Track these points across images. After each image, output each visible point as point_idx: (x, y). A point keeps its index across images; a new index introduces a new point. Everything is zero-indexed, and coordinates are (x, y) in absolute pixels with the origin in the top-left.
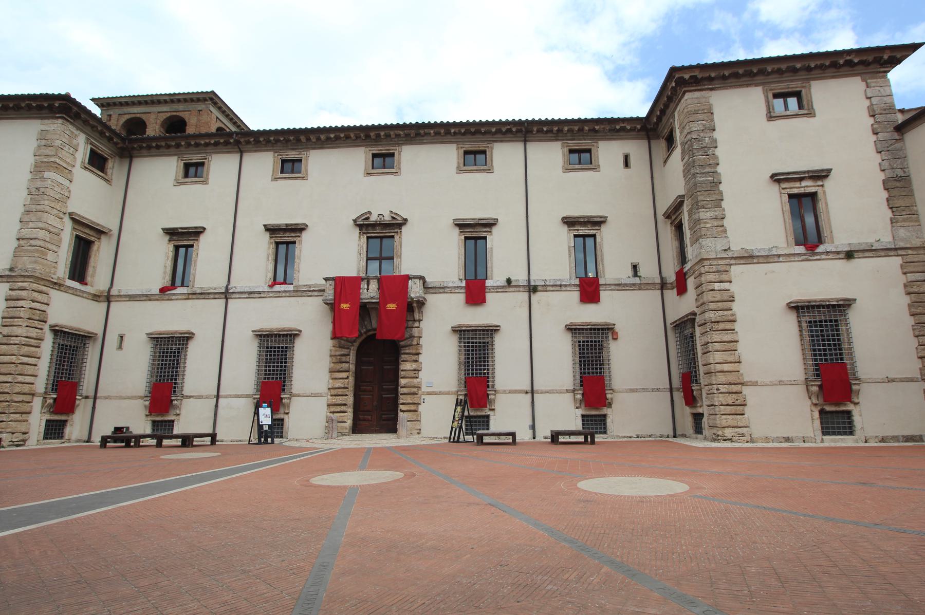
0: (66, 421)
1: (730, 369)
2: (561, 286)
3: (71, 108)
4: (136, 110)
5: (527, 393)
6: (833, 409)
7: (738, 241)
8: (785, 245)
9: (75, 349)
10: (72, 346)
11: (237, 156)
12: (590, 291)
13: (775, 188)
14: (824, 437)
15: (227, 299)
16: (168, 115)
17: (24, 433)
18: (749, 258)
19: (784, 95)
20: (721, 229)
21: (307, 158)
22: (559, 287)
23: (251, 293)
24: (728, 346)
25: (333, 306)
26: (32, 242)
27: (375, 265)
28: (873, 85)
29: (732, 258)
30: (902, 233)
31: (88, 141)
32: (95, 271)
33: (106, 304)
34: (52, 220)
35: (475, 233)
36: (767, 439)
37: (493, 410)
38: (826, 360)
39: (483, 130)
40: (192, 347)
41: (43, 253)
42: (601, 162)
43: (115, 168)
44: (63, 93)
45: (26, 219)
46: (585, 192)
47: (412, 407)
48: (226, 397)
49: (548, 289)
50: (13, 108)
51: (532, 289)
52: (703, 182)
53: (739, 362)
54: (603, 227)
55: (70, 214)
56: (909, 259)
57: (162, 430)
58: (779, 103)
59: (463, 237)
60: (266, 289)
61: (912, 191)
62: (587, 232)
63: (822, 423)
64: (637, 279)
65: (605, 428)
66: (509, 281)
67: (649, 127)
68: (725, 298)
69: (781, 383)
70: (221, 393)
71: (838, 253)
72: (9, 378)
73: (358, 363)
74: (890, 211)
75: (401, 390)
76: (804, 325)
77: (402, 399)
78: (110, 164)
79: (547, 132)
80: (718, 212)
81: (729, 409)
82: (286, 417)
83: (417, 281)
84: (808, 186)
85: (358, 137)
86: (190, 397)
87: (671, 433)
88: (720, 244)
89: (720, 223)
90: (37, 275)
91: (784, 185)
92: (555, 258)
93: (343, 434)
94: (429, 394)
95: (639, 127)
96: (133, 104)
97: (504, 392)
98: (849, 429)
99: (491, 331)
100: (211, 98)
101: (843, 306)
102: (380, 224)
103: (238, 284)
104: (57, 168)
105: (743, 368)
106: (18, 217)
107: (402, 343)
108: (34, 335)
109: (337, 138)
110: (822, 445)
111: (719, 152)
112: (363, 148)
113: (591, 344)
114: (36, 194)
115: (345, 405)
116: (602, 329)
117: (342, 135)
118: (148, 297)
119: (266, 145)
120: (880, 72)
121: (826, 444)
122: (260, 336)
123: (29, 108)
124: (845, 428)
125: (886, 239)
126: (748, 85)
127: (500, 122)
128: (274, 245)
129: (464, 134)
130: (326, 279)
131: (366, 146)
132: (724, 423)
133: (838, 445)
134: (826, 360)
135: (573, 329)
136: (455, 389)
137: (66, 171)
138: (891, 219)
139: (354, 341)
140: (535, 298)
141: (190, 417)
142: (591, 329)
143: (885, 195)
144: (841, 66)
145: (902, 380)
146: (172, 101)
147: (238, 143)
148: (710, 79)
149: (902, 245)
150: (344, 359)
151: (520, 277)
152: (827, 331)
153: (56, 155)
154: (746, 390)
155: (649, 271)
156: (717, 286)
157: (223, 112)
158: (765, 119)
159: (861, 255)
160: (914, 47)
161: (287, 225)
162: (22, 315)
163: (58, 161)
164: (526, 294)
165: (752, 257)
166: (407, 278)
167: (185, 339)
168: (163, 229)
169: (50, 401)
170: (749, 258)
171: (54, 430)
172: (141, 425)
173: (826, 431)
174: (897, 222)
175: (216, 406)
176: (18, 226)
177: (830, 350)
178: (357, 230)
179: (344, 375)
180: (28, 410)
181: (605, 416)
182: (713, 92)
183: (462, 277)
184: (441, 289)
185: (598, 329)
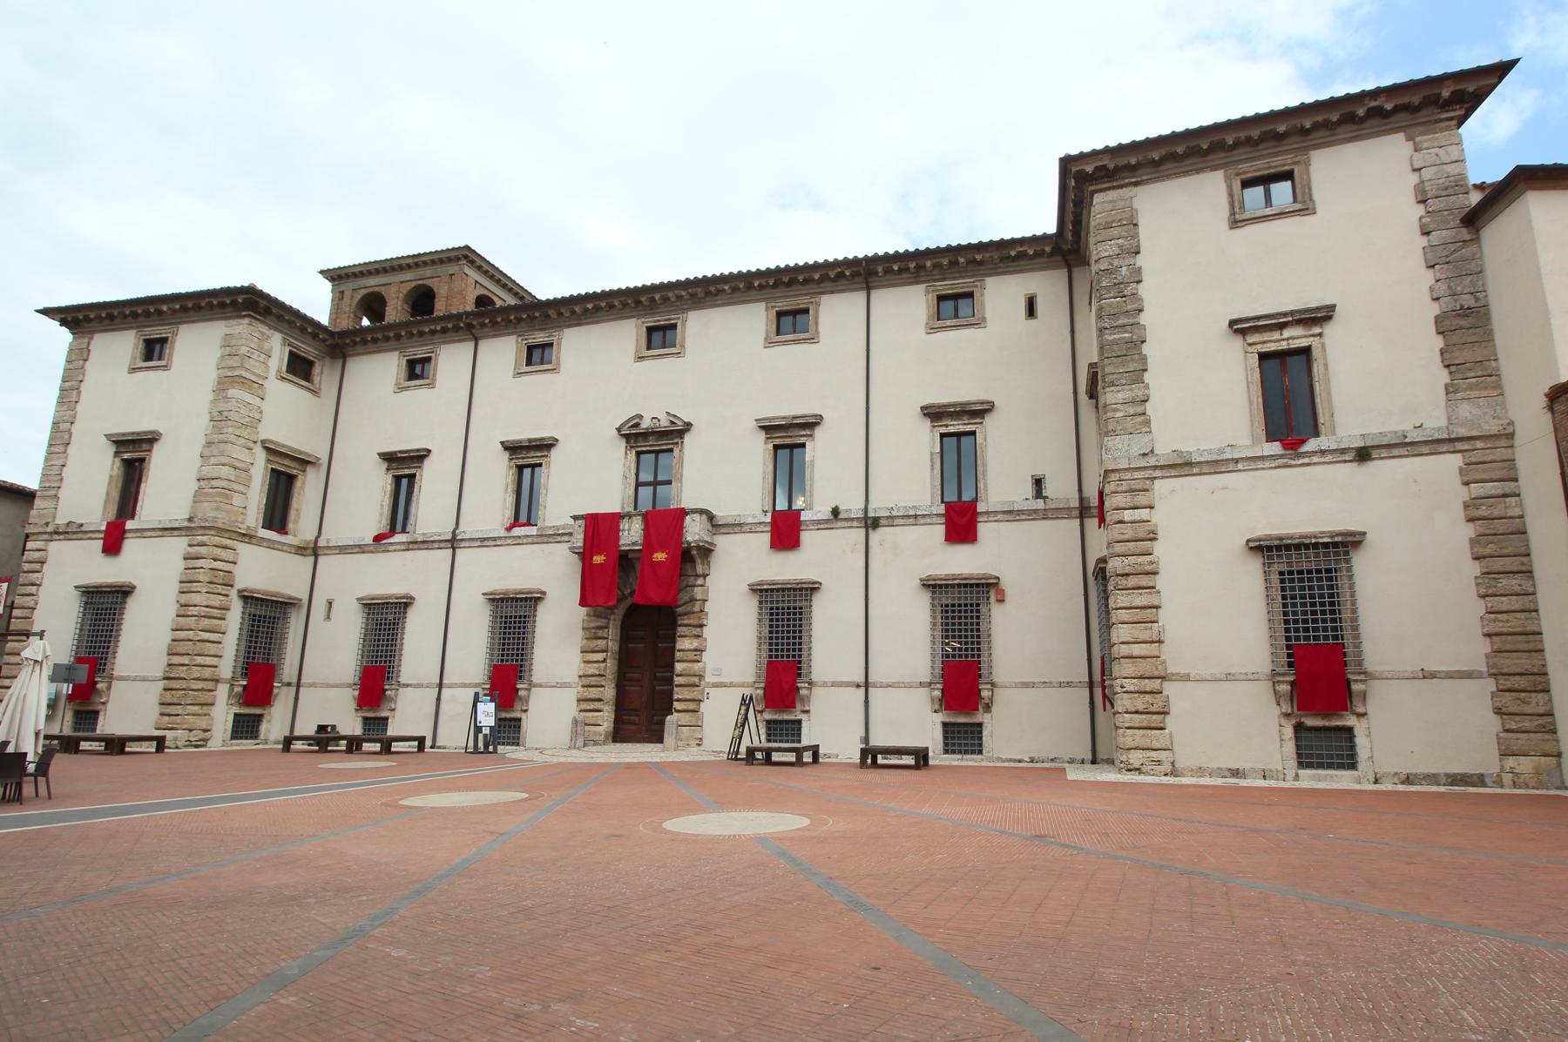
0: (261, 716)
1: (1143, 653)
2: (916, 516)
4: (373, 282)
7: (1168, 438)
8: (1248, 442)
10: (268, 616)
12: (961, 523)
13: (1237, 343)
15: (454, 549)
16: (413, 284)
17: (206, 731)
18: (1184, 466)
20: (1140, 419)
21: (560, 340)
22: (914, 518)
24: (1141, 615)
25: (585, 556)
26: (214, 483)
27: (646, 492)
28: (1425, 145)
29: (1155, 467)
30: (1465, 410)
32: (298, 516)
33: (312, 559)
34: (237, 452)
35: (788, 439)
36: (1200, 771)
37: (807, 712)
39: (801, 278)
40: (412, 614)
41: (226, 496)
42: (988, 315)
43: (325, 375)
46: (955, 364)
47: (691, 706)
48: (452, 686)
49: (897, 522)
51: (871, 523)
52: (1115, 342)
53: (1160, 642)
54: (988, 419)
55: (263, 442)
56: (1476, 457)
57: (374, 727)
58: (1255, 194)
59: (770, 446)
60: (503, 533)
61: (1490, 333)
64: (1040, 501)
65: (980, 745)
66: (835, 512)
67: (1065, 247)
68: (1141, 536)
69: (1229, 677)
71: (1343, 451)
72: (185, 660)
73: (625, 639)
74: (1446, 371)
75: (678, 680)
76: (1275, 577)
77: (678, 693)
78: (317, 369)
79: (900, 271)
80: (1138, 391)
82: (523, 716)
83: (697, 517)
84: (1296, 337)
85: (625, 305)
86: (407, 686)
87: (1089, 757)
88: (1137, 445)
89: (1139, 409)
91: (1251, 339)
92: (910, 474)
93: (596, 743)
94: (715, 685)
95: (1048, 249)
96: (370, 273)
97: (825, 684)
98: (1348, 761)
99: (809, 590)
100: (466, 256)
101: (1346, 544)
102: (654, 433)
103: (469, 528)
104: (243, 382)
105: (1166, 652)
106: (198, 449)
107: (679, 610)
108: (216, 603)
109: (597, 309)
110: (1297, 784)
111: (1144, 290)
113: (962, 608)
114: (219, 419)
116: (978, 585)
118: (360, 549)
119: (506, 327)
120: (1441, 120)
122: (493, 600)
123: (211, 306)
124: (1340, 756)
125: (1435, 421)
126: (1198, 171)
127: (827, 264)
128: (514, 470)
130: (575, 518)
131: (638, 317)
132: (1129, 742)
133: (1322, 785)
134: (1307, 638)
135: (933, 586)
138: (1447, 386)
139: (615, 607)
140: (875, 536)
142: (959, 585)
143: (1439, 342)
145: (1450, 675)
147: (470, 327)
148: (1132, 169)
150: (600, 633)
153: (242, 367)
154: (1170, 689)
155: (1061, 488)
156: (1128, 515)
157: (486, 273)
158: (1225, 224)
159: (1384, 453)
161: (530, 440)
162: (201, 578)
163: (244, 374)
165: (1189, 464)
166: (683, 513)
167: (404, 604)
170: (1184, 466)
171: (246, 727)
172: (350, 724)
173: (1305, 760)
174: (1455, 392)
175: (439, 699)
177: (1324, 621)
178: (623, 443)
179: (600, 656)
180: (210, 700)
181: (980, 725)
183: (768, 507)
184: (737, 527)
185: (972, 585)
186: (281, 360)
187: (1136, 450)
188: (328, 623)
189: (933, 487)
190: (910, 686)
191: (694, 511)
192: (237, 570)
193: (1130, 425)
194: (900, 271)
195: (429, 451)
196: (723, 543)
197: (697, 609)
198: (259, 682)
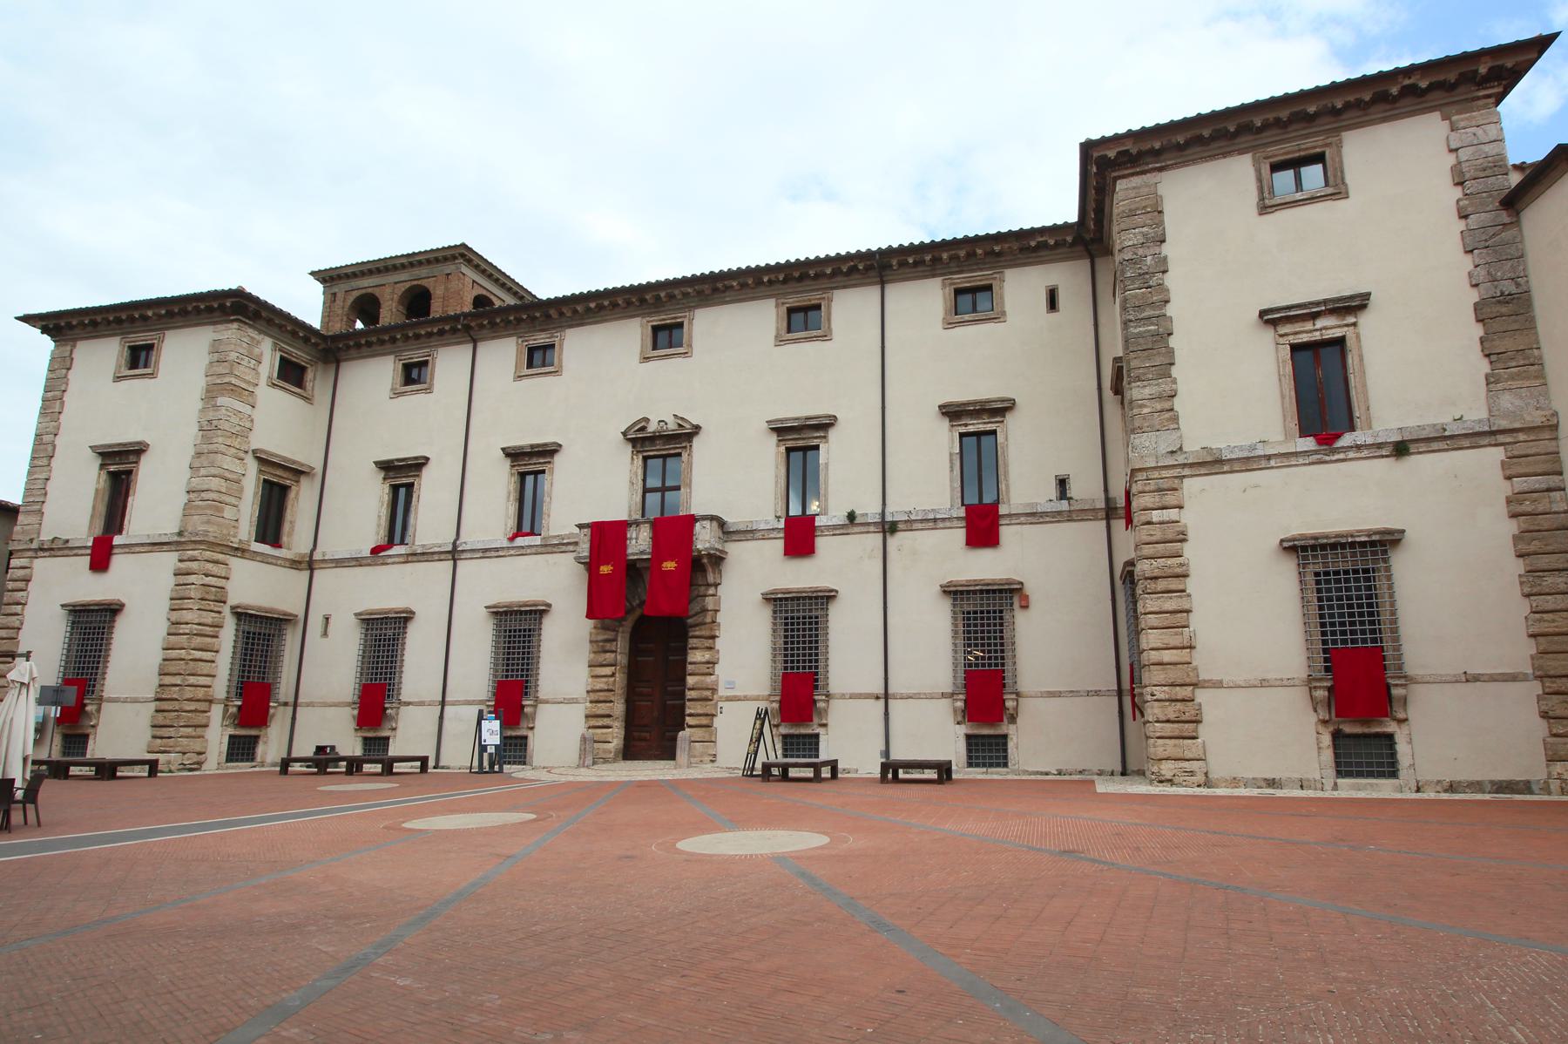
0: (257, 738)
2: (935, 520)
3: (246, 307)
4: (367, 283)
5: (878, 698)
6: (1358, 730)
8: (1281, 438)
9: (268, 638)
10: (262, 634)
11: (470, 347)
12: (982, 527)
13: (1268, 334)
14: (1340, 781)
15: (455, 560)
16: (408, 285)
17: (200, 753)
18: (1214, 464)
19: (1296, 164)
20: (1167, 415)
21: (562, 341)
23: (486, 550)
24: (1172, 620)
25: (592, 566)
28: (1462, 124)
29: (1184, 466)
30: (1507, 401)
31: (275, 347)
32: (292, 529)
34: (229, 463)
35: (801, 441)
36: (1235, 782)
37: (825, 725)
38: (1344, 642)
40: (412, 629)
42: (1008, 308)
43: (317, 380)
44: (234, 287)
45: (197, 464)
46: (976, 359)
47: (704, 721)
48: (454, 703)
49: (915, 526)
50: (179, 313)
51: (888, 528)
52: (1140, 335)
53: (1191, 647)
54: (1009, 417)
55: (254, 452)
56: (1518, 450)
57: (376, 747)
58: (1285, 179)
59: (782, 449)
60: (506, 544)
62: (982, 427)
63: (1336, 755)
64: (1065, 502)
65: (1006, 757)
66: (851, 516)
67: (1088, 237)
68: (1170, 536)
69: (1264, 684)
70: (448, 699)
71: (1379, 446)
72: (178, 680)
74: (1486, 361)
75: (690, 694)
76: (1310, 578)
78: (309, 375)
80: (1165, 387)
81: (1169, 729)
82: (530, 734)
83: (707, 523)
84: (1328, 327)
85: (629, 303)
87: (1119, 768)
88: (1165, 442)
89: (1167, 405)
90: (211, 539)
91: (1283, 330)
92: (928, 476)
93: (606, 761)
94: (729, 699)
95: (1069, 239)
97: (843, 696)
98: (1390, 770)
99: (825, 598)
100: (462, 254)
101: (1384, 543)
102: (661, 437)
103: (470, 539)
105: (1198, 658)
108: (209, 621)
109: (600, 308)
111: (1170, 280)
112: (638, 320)
113: (984, 615)
114: (208, 429)
115: (609, 716)
117: (606, 303)
118: (357, 562)
120: (1478, 98)
121: (1341, 794)
122: (496, 613)
123: (198, 311)
124: (1380, 764)
125: (1475, 412)
126: (1225, 155)
127: (839, 258)
128: (516, 478)
129: (785, 281)
130: (580, 526)
131: (642, 315)
133: (1361, 795)
136: (767, 693)
137: (244, 393)
138: (1487, 377)
140: (893, 542)
141: (409, 733)
142: (981, 591)
143: (1478, 331)
144: (1395, 99)
145: (1493, 678)
146: (412, 265)
147: (467, 328)
148: (1156, 154)
149: (1504, 424)
150: (608, 646)
151: (869, 508)
152: (1358, 589)
154: (1202, 696)
155: (1086, 488)
156: (1156, 516)
157: (484, 272)
158: (1255, 211)
160: (1542, 43)
161: (532, 446)
163: (234, 381)
164: (880, 536)
166: (692, 520)
167: (403, 619)
168: (376, 463)
169: (233, 710)
170: (1214, 464)
171: (241, 749)
172: (350, 745)
174: (1497, 382)
175: (441, 717)
176: (187, 473)
177: (1362, 623)
178: (629, 448)
179: (608, 671)
180: (204, 722)
182: (1164, 174)
183: (781, 513)
184: (749, 534)
185: (994, 591)
186: (272, 366)
187: (1163, 448)
188: (325, 640)
189: (952, 489)
190: (930, 697)
191: (704, 518)
192: (229, 585)
193: (1156, 422)
194: (916, 264)
195: (427, 459)
196: (735, 550)
197: (708, 620)
198: (254, 702)
